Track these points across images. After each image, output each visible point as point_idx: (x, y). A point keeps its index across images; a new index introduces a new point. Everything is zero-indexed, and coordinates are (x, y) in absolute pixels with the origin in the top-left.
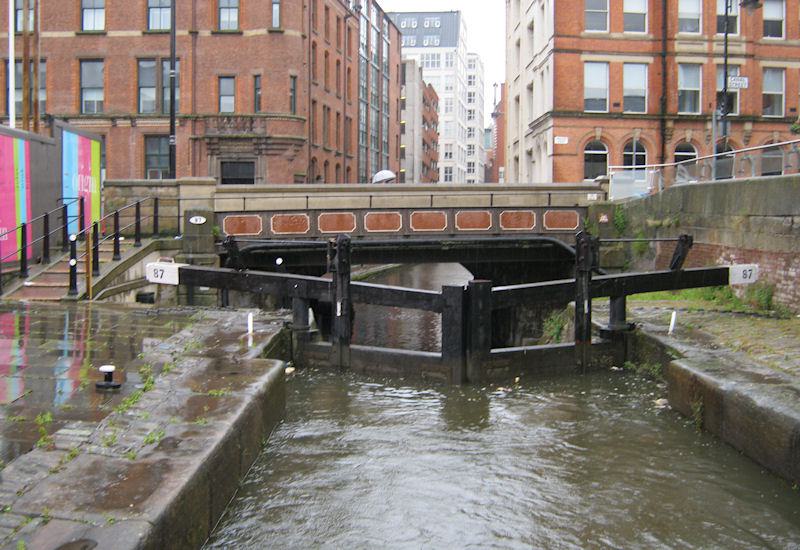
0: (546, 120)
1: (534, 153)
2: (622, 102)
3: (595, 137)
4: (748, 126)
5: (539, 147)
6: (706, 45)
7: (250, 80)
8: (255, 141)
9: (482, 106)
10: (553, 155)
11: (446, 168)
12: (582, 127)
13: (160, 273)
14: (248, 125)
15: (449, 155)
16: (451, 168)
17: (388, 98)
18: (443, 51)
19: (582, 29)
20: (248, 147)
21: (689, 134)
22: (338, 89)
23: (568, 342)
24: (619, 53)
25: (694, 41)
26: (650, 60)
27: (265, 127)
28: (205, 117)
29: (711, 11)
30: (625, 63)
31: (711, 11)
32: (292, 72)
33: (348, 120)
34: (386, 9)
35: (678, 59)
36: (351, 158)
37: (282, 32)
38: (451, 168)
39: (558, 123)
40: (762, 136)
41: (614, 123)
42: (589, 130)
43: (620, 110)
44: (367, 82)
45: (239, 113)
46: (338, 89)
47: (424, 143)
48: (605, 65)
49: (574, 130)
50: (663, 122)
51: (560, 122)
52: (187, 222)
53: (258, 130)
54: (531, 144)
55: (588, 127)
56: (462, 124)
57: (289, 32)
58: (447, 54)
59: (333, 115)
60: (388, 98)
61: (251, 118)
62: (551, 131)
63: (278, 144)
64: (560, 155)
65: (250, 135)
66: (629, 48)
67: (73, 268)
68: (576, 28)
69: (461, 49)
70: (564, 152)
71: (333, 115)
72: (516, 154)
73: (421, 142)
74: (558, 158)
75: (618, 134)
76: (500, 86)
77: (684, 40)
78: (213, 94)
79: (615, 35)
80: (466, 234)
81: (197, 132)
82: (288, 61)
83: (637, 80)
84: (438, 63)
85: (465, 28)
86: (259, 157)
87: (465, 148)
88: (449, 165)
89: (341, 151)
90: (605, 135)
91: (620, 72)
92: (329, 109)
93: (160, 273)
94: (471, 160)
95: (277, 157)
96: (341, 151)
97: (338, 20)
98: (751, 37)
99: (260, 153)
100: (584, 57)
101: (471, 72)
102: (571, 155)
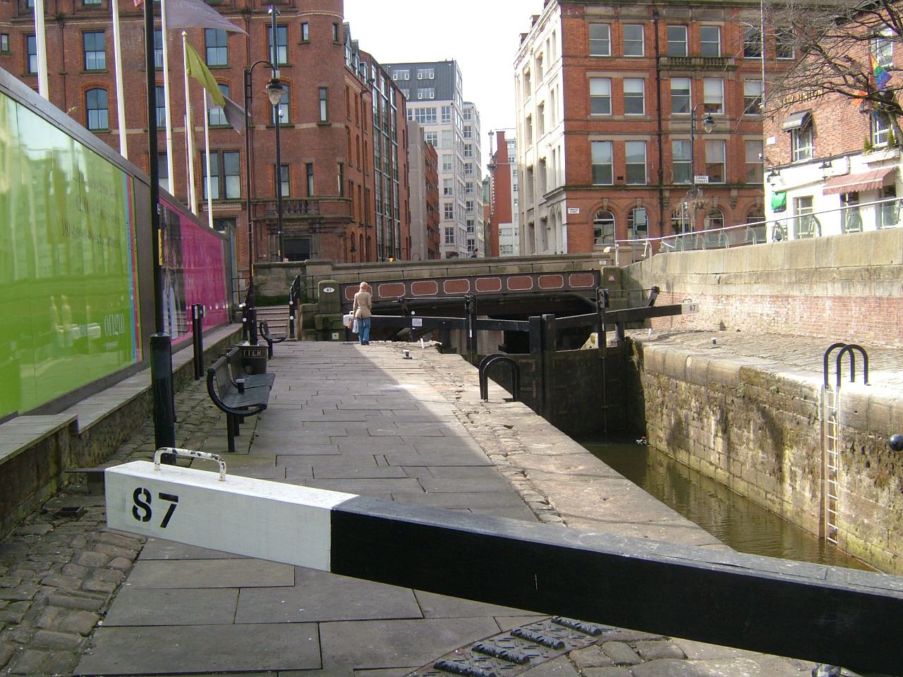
0: (559, 194)
1: (549, 221)
2: (625, 176)
3: (602, 207)
4: (734, 193)
5: (553, 216)
7: (303, 167)
8: (310, 221)
9: (479, 160)
11: (447, 229)
12: (591, 199)
14: (303, 207)
15: (449, 216)
16: (452, 229)
17: (397, 165)
18: (439, 105)
19: (588, 113)
20: (305, 226)
22: (359, 164)
23: (596, 346)
24: (621, 133)
25: (684, 119)
26: (648, 138)
27: (318, 209)
28: (264, 202)
29: (698, 94)
30: (627, 141)
31: (698, 94)
32: (339, 159)
33: (367, 191)
34: (380, 62)
35: (671, 137)
36: (370, 227)
37: (330, 125)
38: (452, 229)
40: (747, 200)
41: (617, 194)
44: (380, 152)
45: (294, 197)
46: (359, 164)
47: (428, 205)
48: (609, 143)
49: (584, 201)
50: (661, 192)
51: (572, 195)
52: (322, 291)
53: (313, 212)
54: (545, 213)
56: (461, 181)
57: (336, 125)
58: (443, 108)
59: (356, 188)
60: (397, 165)
61: (306, 201)
63: (330, 223)
64: (573, 224)
65: (306, 216)
66: (632, 128)
67: (292, 322)
68: (583, 112)
69: (458, 103)
71: (356, 188)
72: (531, 220)
73: (425, 204)
76: (495, 134)
77: (676, 119)
78: (270, 181)
79: (616, 118)
80: (515, 293)
81: (258, 215)
82: (336, 151)
83: (636, 151)
84: (434, 118)
85: (460, 78)
86: (313, 235)
87: (465, 206)
88: (450, 225)
89: (363, 223)
90: (611, 205)
91: (623, 147)
92: (352, 183)
94: (468, 218)
95: (330, 234)
96: (363, 223)
97: (356, 96)
99: (314, 232)
100: (591, 138)
101: (467, 124)
102: (583, 223)
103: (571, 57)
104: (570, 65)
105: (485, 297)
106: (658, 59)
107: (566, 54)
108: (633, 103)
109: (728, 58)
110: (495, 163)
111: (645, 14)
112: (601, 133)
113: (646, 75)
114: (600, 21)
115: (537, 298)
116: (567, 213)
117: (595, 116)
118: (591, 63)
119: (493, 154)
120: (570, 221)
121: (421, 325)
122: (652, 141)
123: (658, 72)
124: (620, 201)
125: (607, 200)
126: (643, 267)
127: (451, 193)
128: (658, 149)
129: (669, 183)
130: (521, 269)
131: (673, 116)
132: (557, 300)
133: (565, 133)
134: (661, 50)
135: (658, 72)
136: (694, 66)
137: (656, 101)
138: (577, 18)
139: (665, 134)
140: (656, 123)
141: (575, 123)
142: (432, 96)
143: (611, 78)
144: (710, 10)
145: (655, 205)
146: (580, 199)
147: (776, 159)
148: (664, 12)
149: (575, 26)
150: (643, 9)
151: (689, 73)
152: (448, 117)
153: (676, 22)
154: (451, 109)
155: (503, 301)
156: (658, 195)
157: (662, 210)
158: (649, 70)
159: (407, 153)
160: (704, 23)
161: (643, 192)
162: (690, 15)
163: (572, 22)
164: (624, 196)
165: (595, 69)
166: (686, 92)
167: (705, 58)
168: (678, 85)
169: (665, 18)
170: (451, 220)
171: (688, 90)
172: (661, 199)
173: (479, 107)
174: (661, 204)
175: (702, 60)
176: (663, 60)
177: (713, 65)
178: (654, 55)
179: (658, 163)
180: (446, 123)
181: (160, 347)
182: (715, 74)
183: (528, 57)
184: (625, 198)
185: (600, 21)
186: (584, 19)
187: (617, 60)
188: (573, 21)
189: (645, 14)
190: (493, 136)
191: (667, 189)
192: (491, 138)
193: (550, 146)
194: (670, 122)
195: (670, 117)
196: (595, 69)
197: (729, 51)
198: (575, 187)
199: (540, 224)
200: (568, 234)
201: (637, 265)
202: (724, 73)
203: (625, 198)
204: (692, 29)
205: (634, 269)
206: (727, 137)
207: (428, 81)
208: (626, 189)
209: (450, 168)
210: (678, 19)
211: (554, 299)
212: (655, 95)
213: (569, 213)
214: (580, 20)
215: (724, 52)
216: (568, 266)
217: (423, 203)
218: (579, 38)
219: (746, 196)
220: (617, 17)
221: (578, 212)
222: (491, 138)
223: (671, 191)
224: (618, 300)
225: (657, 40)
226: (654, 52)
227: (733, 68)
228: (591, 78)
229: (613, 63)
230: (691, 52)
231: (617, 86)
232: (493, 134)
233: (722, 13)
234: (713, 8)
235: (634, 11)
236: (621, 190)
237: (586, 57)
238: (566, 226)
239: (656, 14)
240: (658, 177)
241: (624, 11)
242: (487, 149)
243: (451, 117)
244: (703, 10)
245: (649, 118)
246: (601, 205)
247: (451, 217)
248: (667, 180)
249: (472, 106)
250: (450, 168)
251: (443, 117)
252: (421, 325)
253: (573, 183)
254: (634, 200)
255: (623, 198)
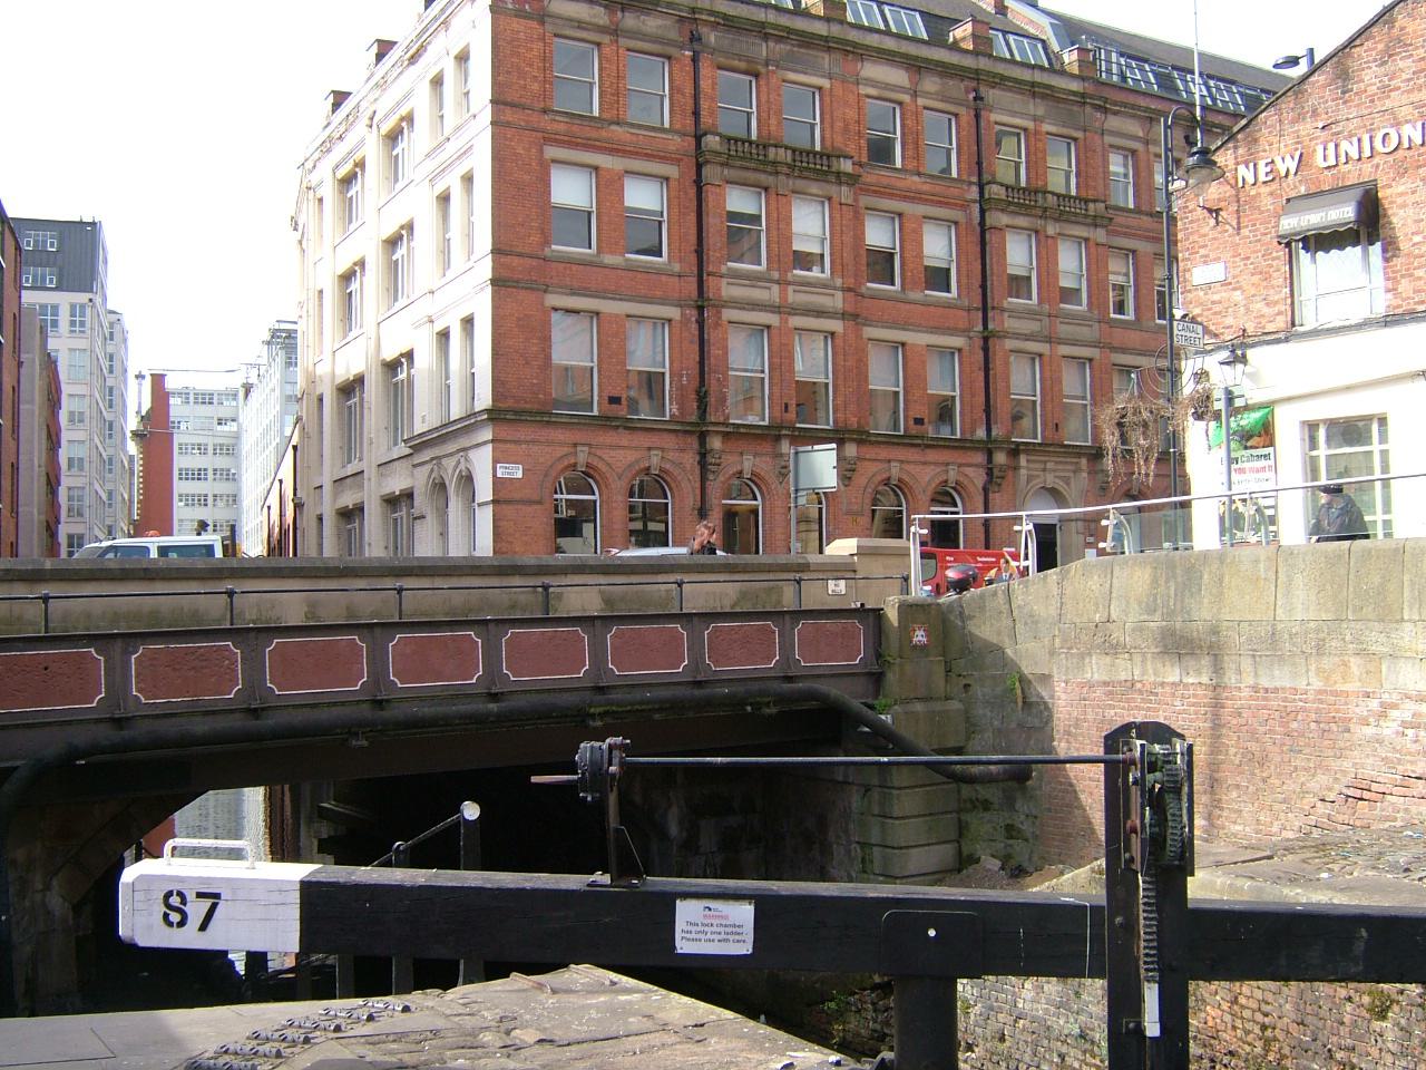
5: (440, 487)
6: (775, 288)
10: (494, 502)
11: (70, 537)
12: (550, 443)
13: (197, 910)
18: (64, 300)
19: (547, 242)
21: (748, 464)
25: (753, 279)
35: (729, 314)
39: (503, 435)
40: (872, 468)
42: (566, 450)
43: (622, 411)
50: (703, 437)
51: (507, 432)
55: (561, 444)
58: (73, 307)
62: (488, 450)
66: (640, 286)
68: (535, 238)
70: (517, 496)
73: (44, 479)
74: (508, 510)
75: (621, 456)
77: (736, 275)
79: (609, 259)
83: (649, 351)
90: (595, 462)
91: (621, 337)
93: (197, 910)
98: (851, 282)
100: (553, 300)
102: (530, 502)
103: (513, 105)
104: (508, 125)
105: (535, 698)
106: (698, 138)
107: (502, 98)
108: (641, 233)
109: (839, 157)
110: (145, 428)
111: (673, 35)
112: (574, 292)
113: (671, 171)
114: (579, 34)
115: (709, 703)
116: (494, 475)
117: (558, 252)
118: (556, 127)
119: (143, 413)
120: (502, 495)
121: (746, 948)
122: (685, 321)
123: (699, 167)
124: (613, 453)
125: (586, 449)
126: (1018, 599)
127: (81, 469)
128: (696, 339)
129: (721, 420)
130: (608, 601)
131: (729, 269)
132: (767, 711)
133: (495, 282)
134: (706, 120)
135: (699, 167)
136: (774, 163)
137: (693, 231)
138: (525, 18)
139: (713, 306)
140: (693, 280)
141: (516, 261)
142: (51, 281)
143: (596, 169)
144: (802, 50)
145: (688, 467)
146: (527, 442)
147: (1229, 321)
148: (712, 39)
149: (522, 35)
150: (668, 22)
151: (763, 178)
152: (82, 324)
153: (736, 63)
154: (88, 310)
155: (602, 715)
156: (696, 445)
157: (703, 479)
158: (679, 160)
159: (20, 364)
160: (792, 76)
161: (665, 436)
162: (764, 54)
163: (515, 26)
164: (625, 442)
165: (564, 142)
166: (755, 219)
167: (794, 151)
168: (739, 201)
169: (713, 51)
170: (79, 519)
171: (760, 216)
172: (703, 455)
173: (128, 323)
174: (703, 464)
175: (789, 152)
176: (712, 141)
177: (813, 167)
178: (691, 129)
179: (697, 371)
180: (77, 335)
181: (973, 79)
182: (814, 188)
183: (360, 127)
184: (624, 447)
185: (579, 34)
186: (542, 23)
187: (613, 127)
188: (518, 25)
189: (673, 35)
190: (143, 382)
191: (717, 432)
192: (140, 384)
193: (432, 322)
194: (725, 281)
195: (724, 269)
196: (564, 142)
197: (839, 141)
198: (516, 412)
199: (379, 509)
200: (495, 527)
201: (995, 594)
202: (833, 190)
203: (624, 447)
204: (768, 84)
205: (982, 608)
206: (836, 326)
207: (44, 254)
208: (629, 426)
209: (81, 421)
210: (740, 57)
211: (757, 706)
212: (692, 217)
213: (499, 475)
214: (534, 24)
215: (828, 143)
216: (743, 595)
217: (39, 476)
218: (531, 65)
219: (869, 460)
220: (615, 32)
221: (520, 475)
222: (140, 384)
223: (726, 435)
224: (937, 706)
225: (696, 97)
226: (690, 121)
227: (852, 180)
228: (554, 161)
229: (604, 134)
230: (765, 133)
231: (609, 188)
232: (143, 377)
233: (826, 60)
234: (807, 45)
235: (652, 24)
236: (618, 427)
237: (545, 111)
238: (491, 507)
239: (695, 38)
240: (695, 405)
241: (630, 21)
242: (137, 399)
243: (88, 325)
244: (788, 47)
245: (677, 267)
246: (573, 461)
247: (80, 514)
248: (717, 410)
249: (117, 317)
250: (81, 421)
251: (73, 323)
252: (746, 948)
253: (509, 404)
254: (646, 452)
255: (620, 447)
